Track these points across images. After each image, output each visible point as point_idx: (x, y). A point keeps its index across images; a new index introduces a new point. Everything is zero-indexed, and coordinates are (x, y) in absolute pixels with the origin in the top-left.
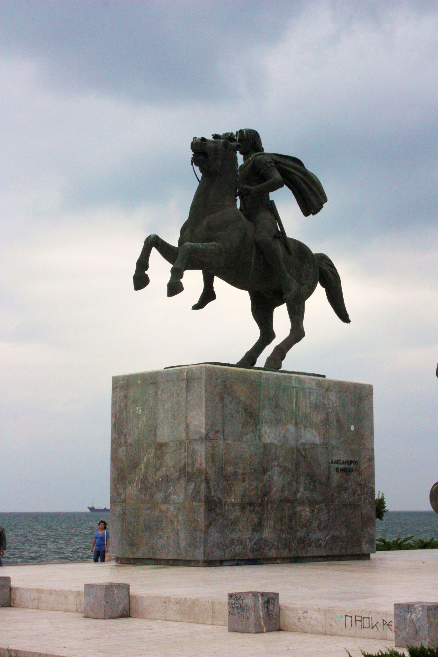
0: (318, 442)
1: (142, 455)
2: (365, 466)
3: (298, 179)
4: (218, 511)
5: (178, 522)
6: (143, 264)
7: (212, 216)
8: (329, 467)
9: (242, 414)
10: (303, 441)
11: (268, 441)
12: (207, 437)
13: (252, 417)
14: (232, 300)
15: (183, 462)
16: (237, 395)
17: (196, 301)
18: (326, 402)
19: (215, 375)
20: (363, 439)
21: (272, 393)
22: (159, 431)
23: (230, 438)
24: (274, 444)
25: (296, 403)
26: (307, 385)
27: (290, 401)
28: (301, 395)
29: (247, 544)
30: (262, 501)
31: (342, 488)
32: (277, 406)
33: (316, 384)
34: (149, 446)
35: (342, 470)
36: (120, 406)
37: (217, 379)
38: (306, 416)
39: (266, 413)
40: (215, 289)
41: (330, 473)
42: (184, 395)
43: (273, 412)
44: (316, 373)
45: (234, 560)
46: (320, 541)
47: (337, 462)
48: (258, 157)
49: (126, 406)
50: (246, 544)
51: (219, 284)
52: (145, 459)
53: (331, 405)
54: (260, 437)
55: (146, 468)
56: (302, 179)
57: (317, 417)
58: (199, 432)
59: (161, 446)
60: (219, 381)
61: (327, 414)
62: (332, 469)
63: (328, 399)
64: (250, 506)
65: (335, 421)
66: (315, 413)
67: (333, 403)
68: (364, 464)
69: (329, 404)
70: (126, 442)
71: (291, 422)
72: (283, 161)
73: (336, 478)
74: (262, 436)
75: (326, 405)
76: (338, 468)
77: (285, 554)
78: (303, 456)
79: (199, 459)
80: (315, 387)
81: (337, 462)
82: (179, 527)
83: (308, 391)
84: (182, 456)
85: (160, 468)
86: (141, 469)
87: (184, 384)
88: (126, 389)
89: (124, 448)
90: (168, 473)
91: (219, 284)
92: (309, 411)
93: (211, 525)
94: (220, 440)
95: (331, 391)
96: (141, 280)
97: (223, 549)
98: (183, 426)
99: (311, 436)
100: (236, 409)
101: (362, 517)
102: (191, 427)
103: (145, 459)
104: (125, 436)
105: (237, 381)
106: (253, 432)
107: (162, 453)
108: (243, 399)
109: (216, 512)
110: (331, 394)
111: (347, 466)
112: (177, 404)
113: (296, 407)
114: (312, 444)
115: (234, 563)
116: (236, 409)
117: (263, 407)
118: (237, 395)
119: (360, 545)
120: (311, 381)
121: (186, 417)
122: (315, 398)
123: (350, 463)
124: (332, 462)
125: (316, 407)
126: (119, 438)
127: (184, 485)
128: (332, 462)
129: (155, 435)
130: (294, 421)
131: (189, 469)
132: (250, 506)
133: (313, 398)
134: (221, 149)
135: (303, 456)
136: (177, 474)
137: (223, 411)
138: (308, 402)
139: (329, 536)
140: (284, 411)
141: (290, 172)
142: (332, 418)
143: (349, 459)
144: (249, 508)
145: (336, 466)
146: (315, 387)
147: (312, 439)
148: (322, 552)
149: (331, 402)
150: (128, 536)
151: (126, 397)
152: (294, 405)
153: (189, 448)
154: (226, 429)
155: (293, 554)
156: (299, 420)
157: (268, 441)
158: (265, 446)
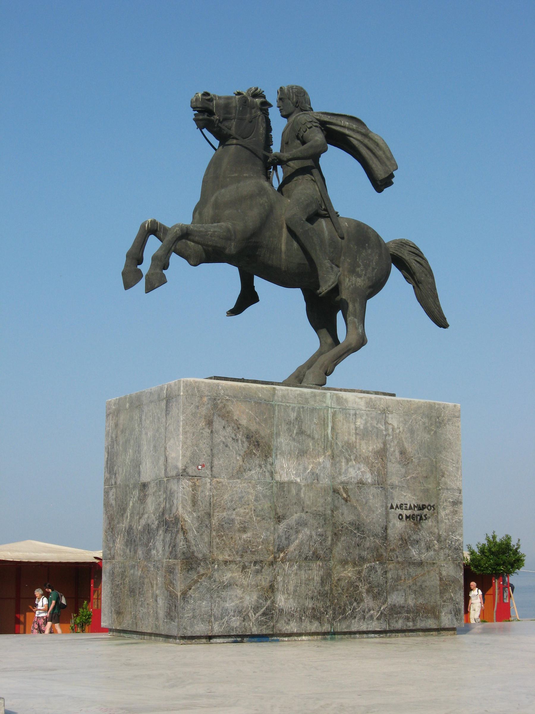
0: (369, 481)
1: (128, 499)
2: (447, 511)
3: (355, 142)
4: (202, 571)
5: (157, 584)
6: (135, 257)
7: (223, 191)
8: (387, 514)
9: (243, 442)
10: (343, 478)
11: (286, 479)
12: (185, 473)
13: (259, 446)
14: (282, 305)
15: (162, 506)
16: (235, 418)
17: (232, 306)
18: (383, 428)
19: (199, 391)
20: (443, 476)
21: (293, 416)
22: (143, 468)
23: (223, 475)
24: (296, 483)
25: (333, 428)
26: (350, 405)
27: (324, 425)
28: (340, 417)
29: (250, 615)
30: (275, 558)
31: (405, 542)
32: (301, 432)
33: (367, 403)
34: (134, 487)
35: (407, 517)
36: (112, 437)
37: (201, 397)
38: (350, 447)
39: (283, 441)
40: (256, 289)
41: (388, 521)
42: (164, 420)
43: (294, 439)
44: (364, 390)
45: (230, 636)
46: (372, 612)
47: (401, 507)
48: (298, 118)
49: (116, 437)
50: (247, 615)
51: (260, 284)
52: (131, 504)
53: (390, 431)
54: (272, 474)
55: (132, 516)
56: (361, 142)
57: (367, 448)
58: (176, 467)
59: (144, 486)
60: (205, 399)
61: (385, 444)
62: (391, 516)
63: (386, 423)
64: (255, 565)
65: (397, 453)
66: (363, 443)
67: (393, 429)
68: (444, 509)
69: (387, 430)
70: (116, 483)
71: (324, 453)
72: (334, 120)
73: (398, 527)
74: (276, 473)
75: (382, 430)
76: (400, 515)
77: (314, 627)
78: (344, 498)
79: (175, 501)
80: (364, 408)
81: (401, 507)
82: (158, 592)
83: (352, 412)
84: (162, 499)
85: (143, 514)
86: (127, 517)
87: (163, 404)
88: (117, 416)
89: (114, 490)
90: (149, 522)
91: (260, 284)
92: (354, 439)
93: (190, 589)
94: (205, 477)
95: (392, 413)
96: (130, 278)
97: (209, 622)
98: (162, 459)
99: (354, 472)
100: (233, 436)
101: (441, 579)
102: (169, 461)
103: (131, 504)
104: (115, 474)
105: (234, 400)
106: (260, 466)
107: (145, 495)
108: (244, 422)
109: (198, 573)
110: (390, 416)
111: (417, 512)
112: (158, 430)
113: (332, 434)
114: (358, 483)
115: (231, 639)
116: (233, 436)
117: (278, 435)
118: (235, 418)
119: (437, 617)
120: (357, 400)
121: (166, 448)
122: (363, 422)
123: (423, 507)
124: (392, 507)
125: (364, 434)
126: (111, 478)
127: (162, 537)
128: (392, 507)
129: (139, 473)
130: (329, 453)
131: (167, 516)
132: (255, 565)
133: (360, 423)
134: (236, 107)
135: (344, 498)
136: (156, 523)
137: (212, 438)
138: (353, 426)
139: (385, 606)
140: (313, 438)
141: (344, 135)
142: (393, 449)
143: (421, 504)
144: (253, 568)
145: (399, 511)
146: (364, 408)
147: (359, 477)
148: (375, 625)
149: (390, 427)
150: (116, 601)
151: (116, 425)
152: (329, 431)
153: (167, 488)
154: (216, 462)
155: (326, 627)
156: (336, 452)
157: (285, 479)
158: (281, 485)
